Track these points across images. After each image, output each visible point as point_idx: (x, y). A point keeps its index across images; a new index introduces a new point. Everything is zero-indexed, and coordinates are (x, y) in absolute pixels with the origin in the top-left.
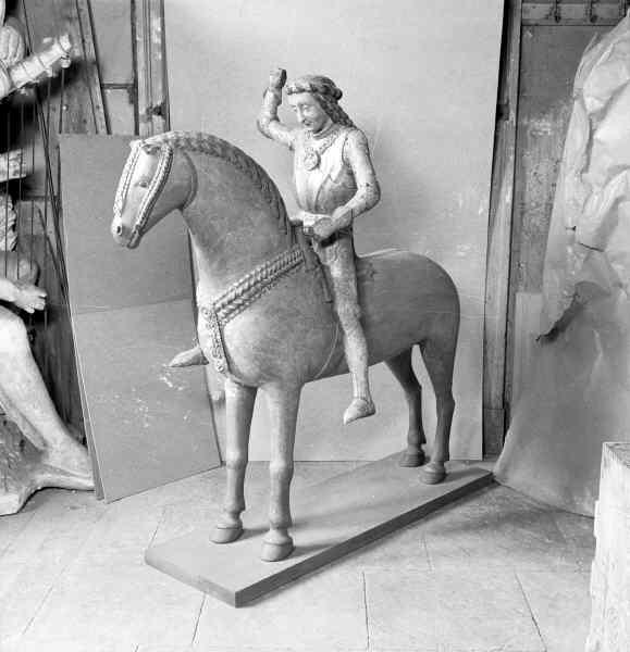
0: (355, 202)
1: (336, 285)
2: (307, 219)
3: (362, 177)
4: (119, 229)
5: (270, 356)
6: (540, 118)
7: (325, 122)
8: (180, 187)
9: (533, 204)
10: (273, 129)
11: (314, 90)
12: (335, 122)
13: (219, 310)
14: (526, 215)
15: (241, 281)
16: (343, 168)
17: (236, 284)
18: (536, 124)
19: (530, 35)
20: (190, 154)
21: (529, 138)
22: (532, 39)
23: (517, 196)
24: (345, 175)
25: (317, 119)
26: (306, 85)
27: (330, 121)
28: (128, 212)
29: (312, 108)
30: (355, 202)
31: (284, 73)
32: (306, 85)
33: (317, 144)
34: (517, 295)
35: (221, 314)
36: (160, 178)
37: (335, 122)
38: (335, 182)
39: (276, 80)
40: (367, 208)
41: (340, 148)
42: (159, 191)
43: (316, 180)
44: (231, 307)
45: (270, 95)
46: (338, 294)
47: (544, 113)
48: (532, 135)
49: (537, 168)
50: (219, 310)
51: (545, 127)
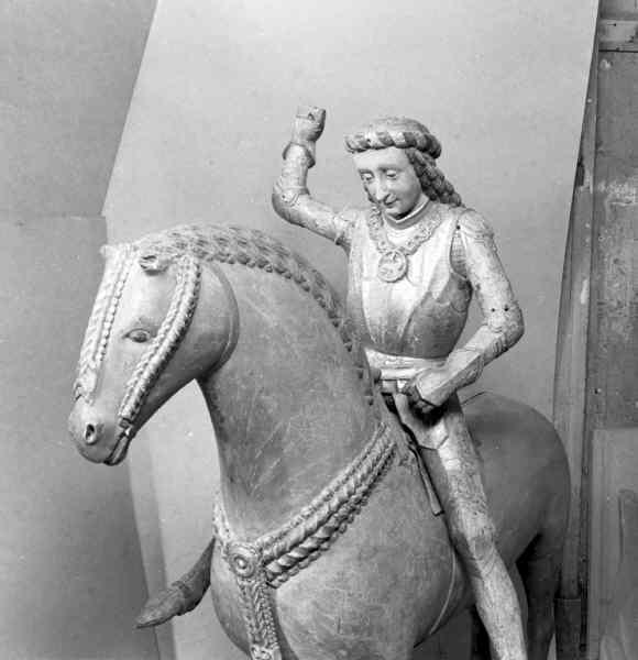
0: (481, 340)
1: (454, 484)
2: (386, 368)
3: (492, 293)
4: (91, 428)
5: (365, 638)
6: (623, 182)
7: (418, 198)
8: (211, 337)
9: (615, 304)
10: (304, 208)
11: (409, 144)
12: (432, 199)
13: (271, 559)
14: (605, 320)
15: (315, 502)
16: (452, 276)
17: (305, 510)
18: (617, 190)
19: (608, 65)
20: (225, 267)
21: (608, 211)
22: (611, 70)
23: (595, 292)
24: (454, 290)
25: (408, 194)
26: (397, 135)
27: (424, 199)
28: (108, 395)
29: (403, 175)
30: (481, 340)
31: (325, 112)
32: (397, 135)
33: (401, 237)
34: (596, 432)
35: (272, 567)
36: (171, 337)
37: (432, 199)
38: (439, 301)
39: (309, 126)
40: (503, 349)
41: (439, 243)
42: (169, 356)
43: (407, 297)
44: (295, 554)
45: (297, 153)
46: (460, 501)
47: (627, 176)
48: (612, 206)
49: (619, 252)
50: (271, 559)
51: (628, 194)
